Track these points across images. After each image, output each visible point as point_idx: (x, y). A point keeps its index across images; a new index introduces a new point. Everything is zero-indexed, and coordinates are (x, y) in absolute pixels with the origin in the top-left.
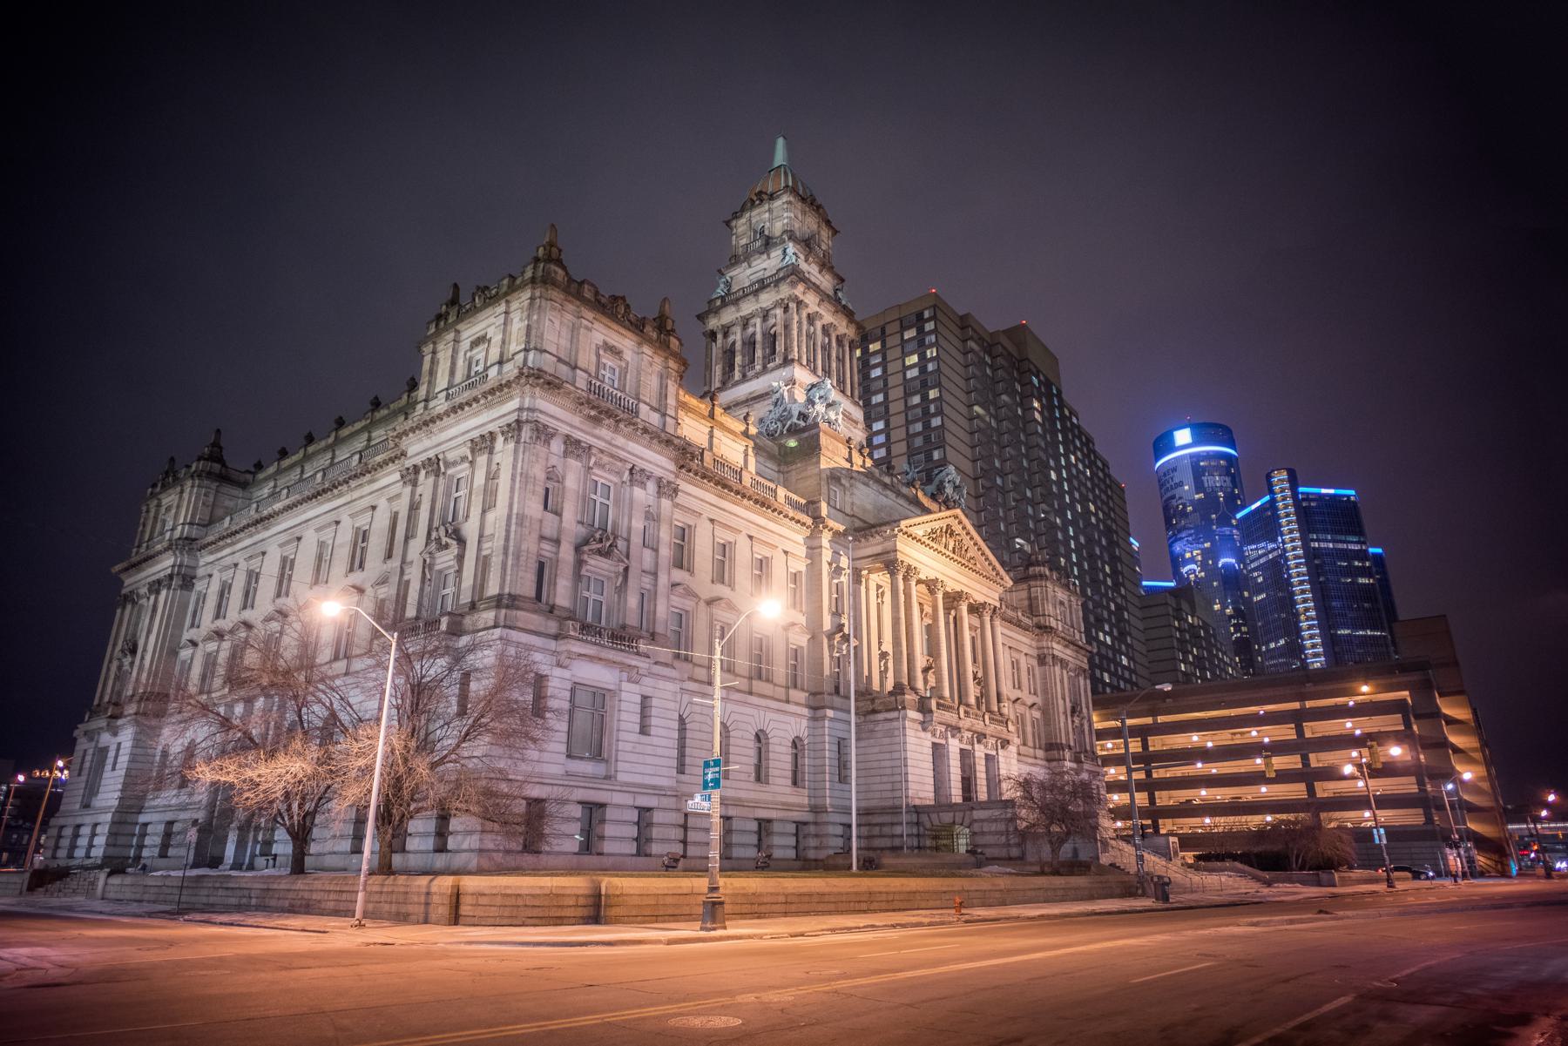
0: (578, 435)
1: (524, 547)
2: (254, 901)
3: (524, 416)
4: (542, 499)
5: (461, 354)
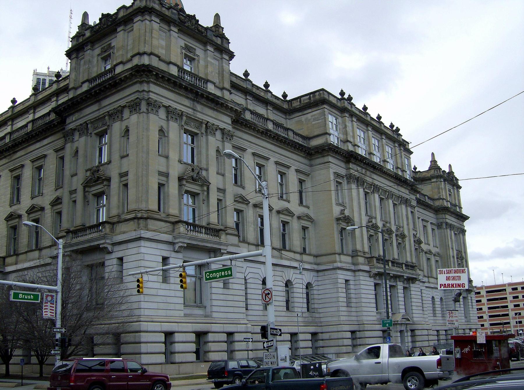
0: (174, 105)
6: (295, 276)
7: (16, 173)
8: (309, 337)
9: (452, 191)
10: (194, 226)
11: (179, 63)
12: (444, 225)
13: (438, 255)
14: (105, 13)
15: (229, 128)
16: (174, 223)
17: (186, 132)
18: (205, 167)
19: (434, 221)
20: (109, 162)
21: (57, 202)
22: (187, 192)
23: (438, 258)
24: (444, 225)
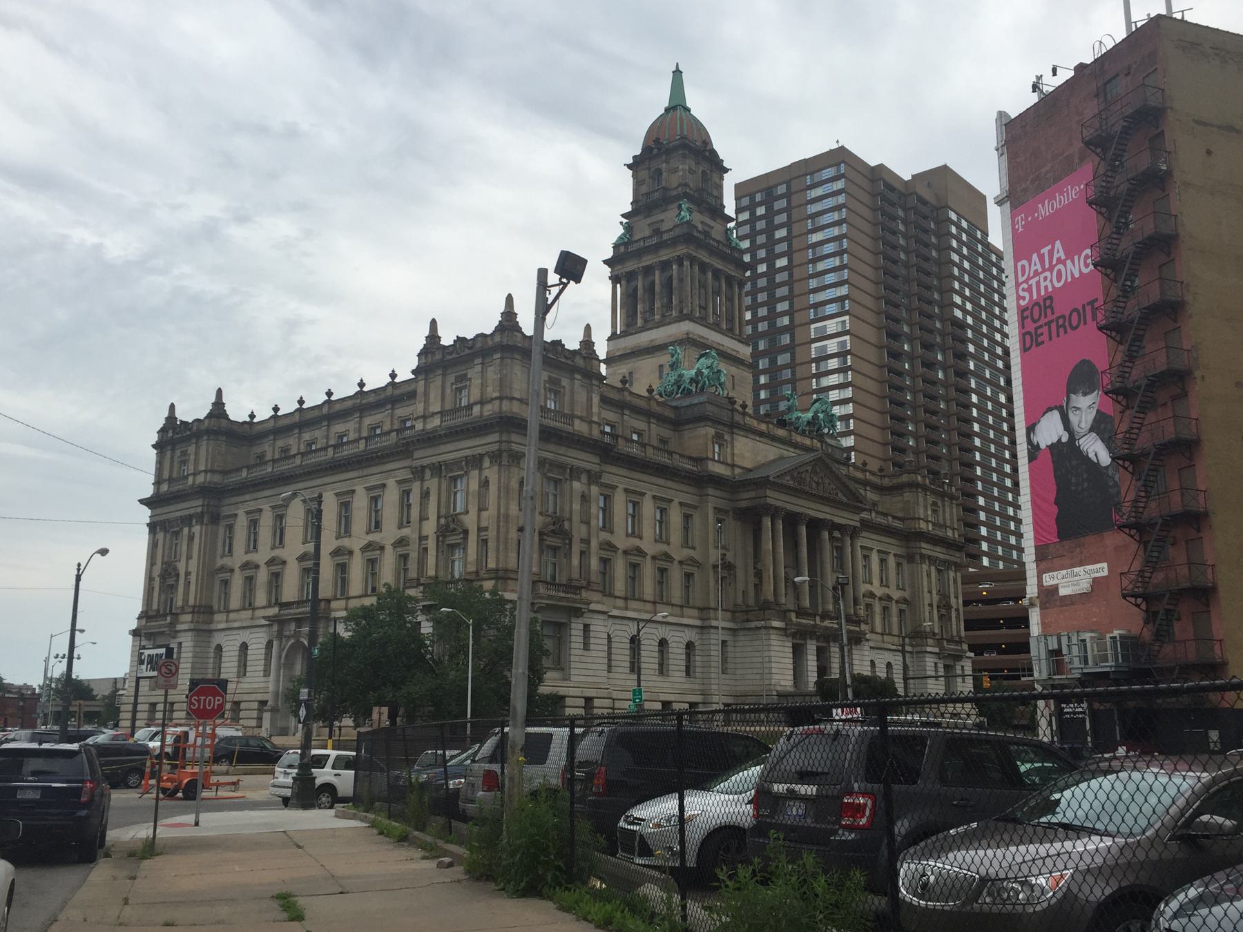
3: (504, 446)
5: (448, 385)
6: (672, 633)
9: (940, 503)
10: (552, 583)
12: (918, 557)
13: (905, 601)
14: (461, 335)
17: (549, 479)
19: (899, 551)
21: (401, 542)
23: (904, 607)
24: (918, 557)
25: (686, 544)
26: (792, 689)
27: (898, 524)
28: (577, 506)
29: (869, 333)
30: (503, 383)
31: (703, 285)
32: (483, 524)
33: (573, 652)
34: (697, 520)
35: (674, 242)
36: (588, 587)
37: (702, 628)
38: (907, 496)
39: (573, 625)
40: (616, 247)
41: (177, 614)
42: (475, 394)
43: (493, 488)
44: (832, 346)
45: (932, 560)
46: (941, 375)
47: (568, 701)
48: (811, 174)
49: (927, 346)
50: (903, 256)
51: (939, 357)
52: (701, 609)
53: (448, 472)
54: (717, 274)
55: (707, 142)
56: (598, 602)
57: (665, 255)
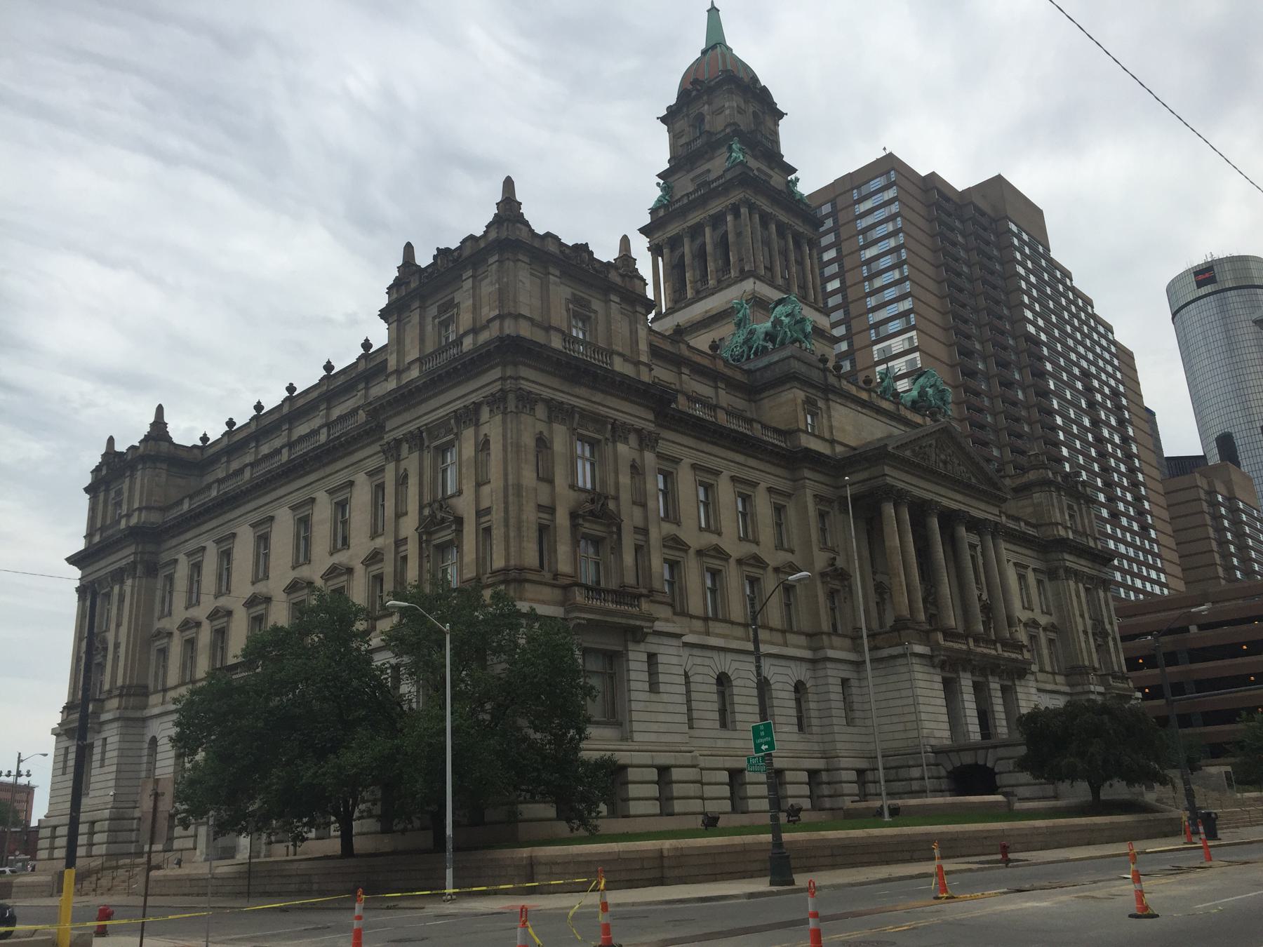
0: (560, 397)
1: (524, 517)
2: (315, 887)
3: (509, 385)
4: (534, 468)
5: (429, 320)
7: (302, 513)
8: (804, 777)
9: (1075, 507)
10: (594, 590)
11: (564, 327)
12: (1061, 572)
15: (651, 427)
16: (565, 588)
17: (582, 439)
18: (613, 493)
19: (1037, 565)
20: (460, 492)
21: (374, 557)
22: (586, 537)
23: (1052, 635)
24: (1061, 572)
25: (780, 546)
26: (948, 742)
27: (1031, 531)
28: (625, 480)
29: (940, 351)
30: (502, 295)
31: (767, 243)
32: (485, 504)
33: (634, 695)
34: (791, 513)
35: (726, 188)
36: (651, 594)
37: (813, 661)
38: (1037, 497)
39: (631, 656)
40: (653, 211)
41: (103, 701)
42: (465, 320)
43: (496, 448)
44: (900, 366)
45: (1078, 576)
46: (1020, 395)
47: (632, 774)
48: (858, 187)
49: (1004, 365)
50: (965, 269)
51: (1017, 376)
52: (809, 635)
53: (434, 441)
54: (782, 229)
55: (755, 79)
56: (667, 620)
57: (715, 207)
